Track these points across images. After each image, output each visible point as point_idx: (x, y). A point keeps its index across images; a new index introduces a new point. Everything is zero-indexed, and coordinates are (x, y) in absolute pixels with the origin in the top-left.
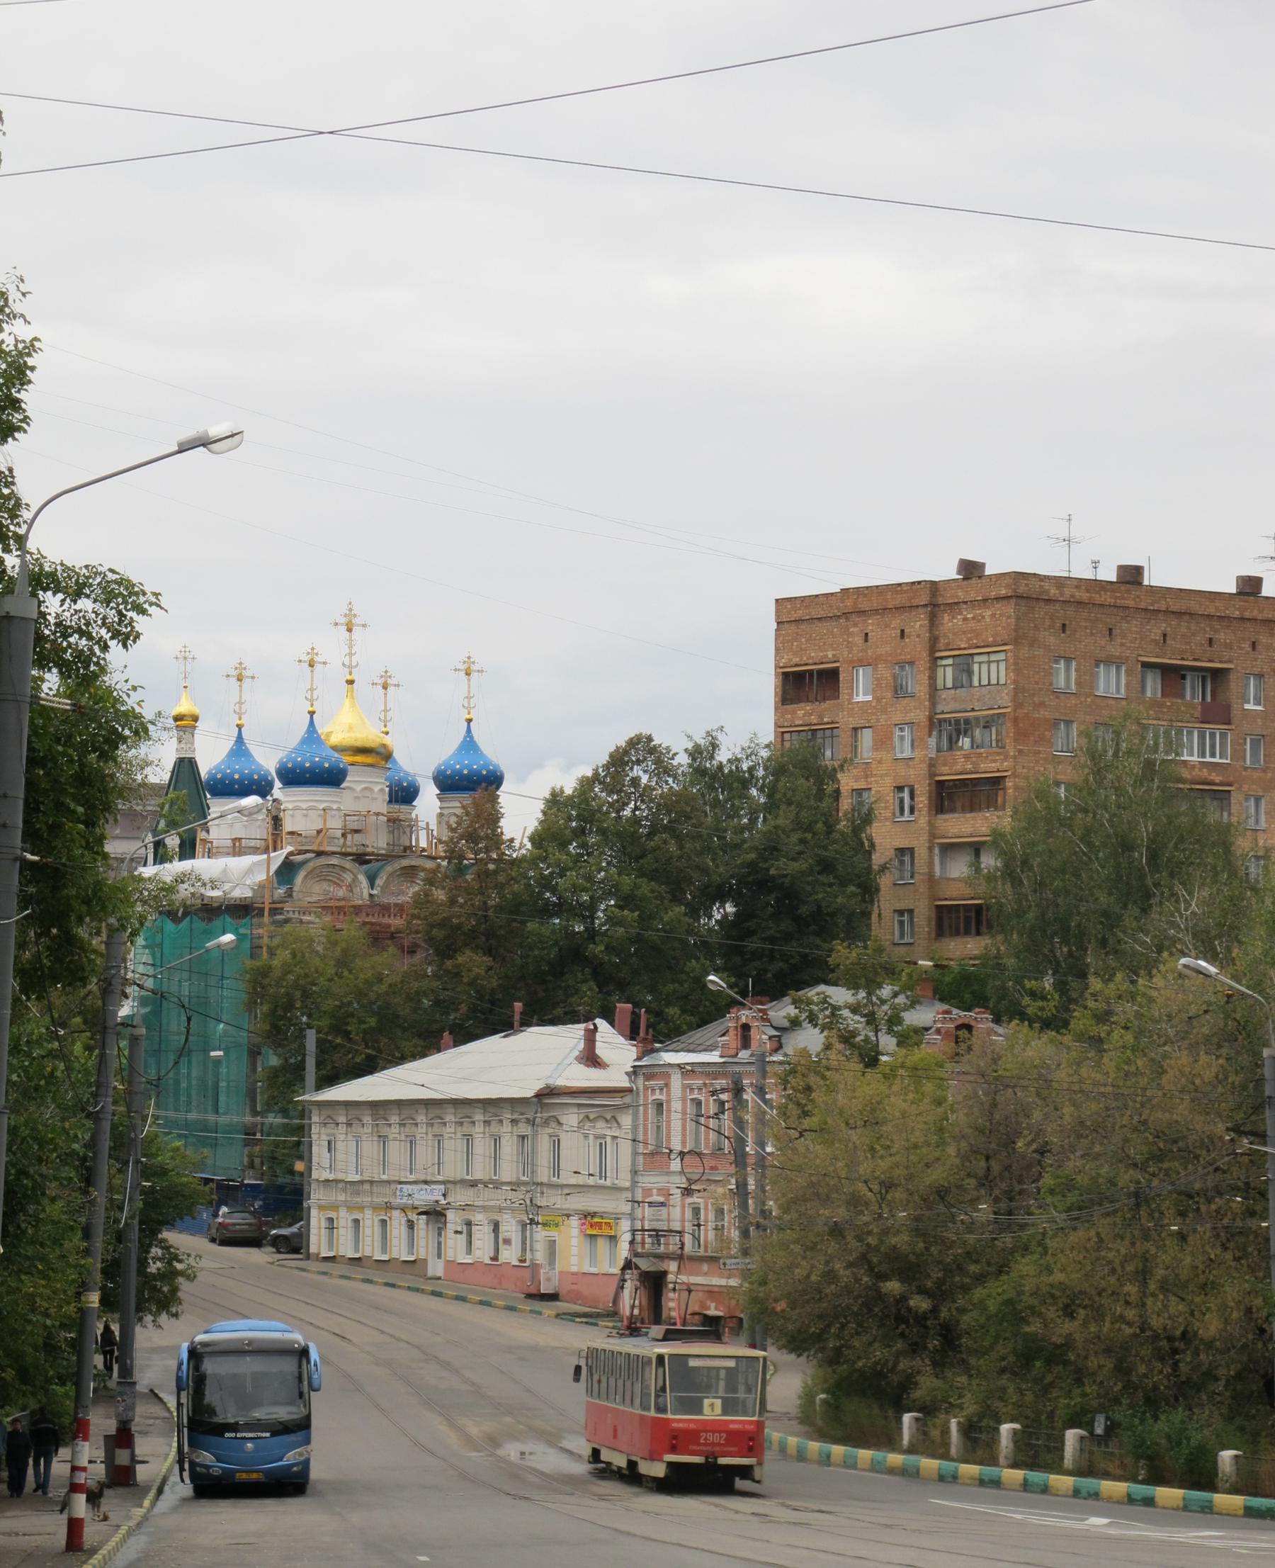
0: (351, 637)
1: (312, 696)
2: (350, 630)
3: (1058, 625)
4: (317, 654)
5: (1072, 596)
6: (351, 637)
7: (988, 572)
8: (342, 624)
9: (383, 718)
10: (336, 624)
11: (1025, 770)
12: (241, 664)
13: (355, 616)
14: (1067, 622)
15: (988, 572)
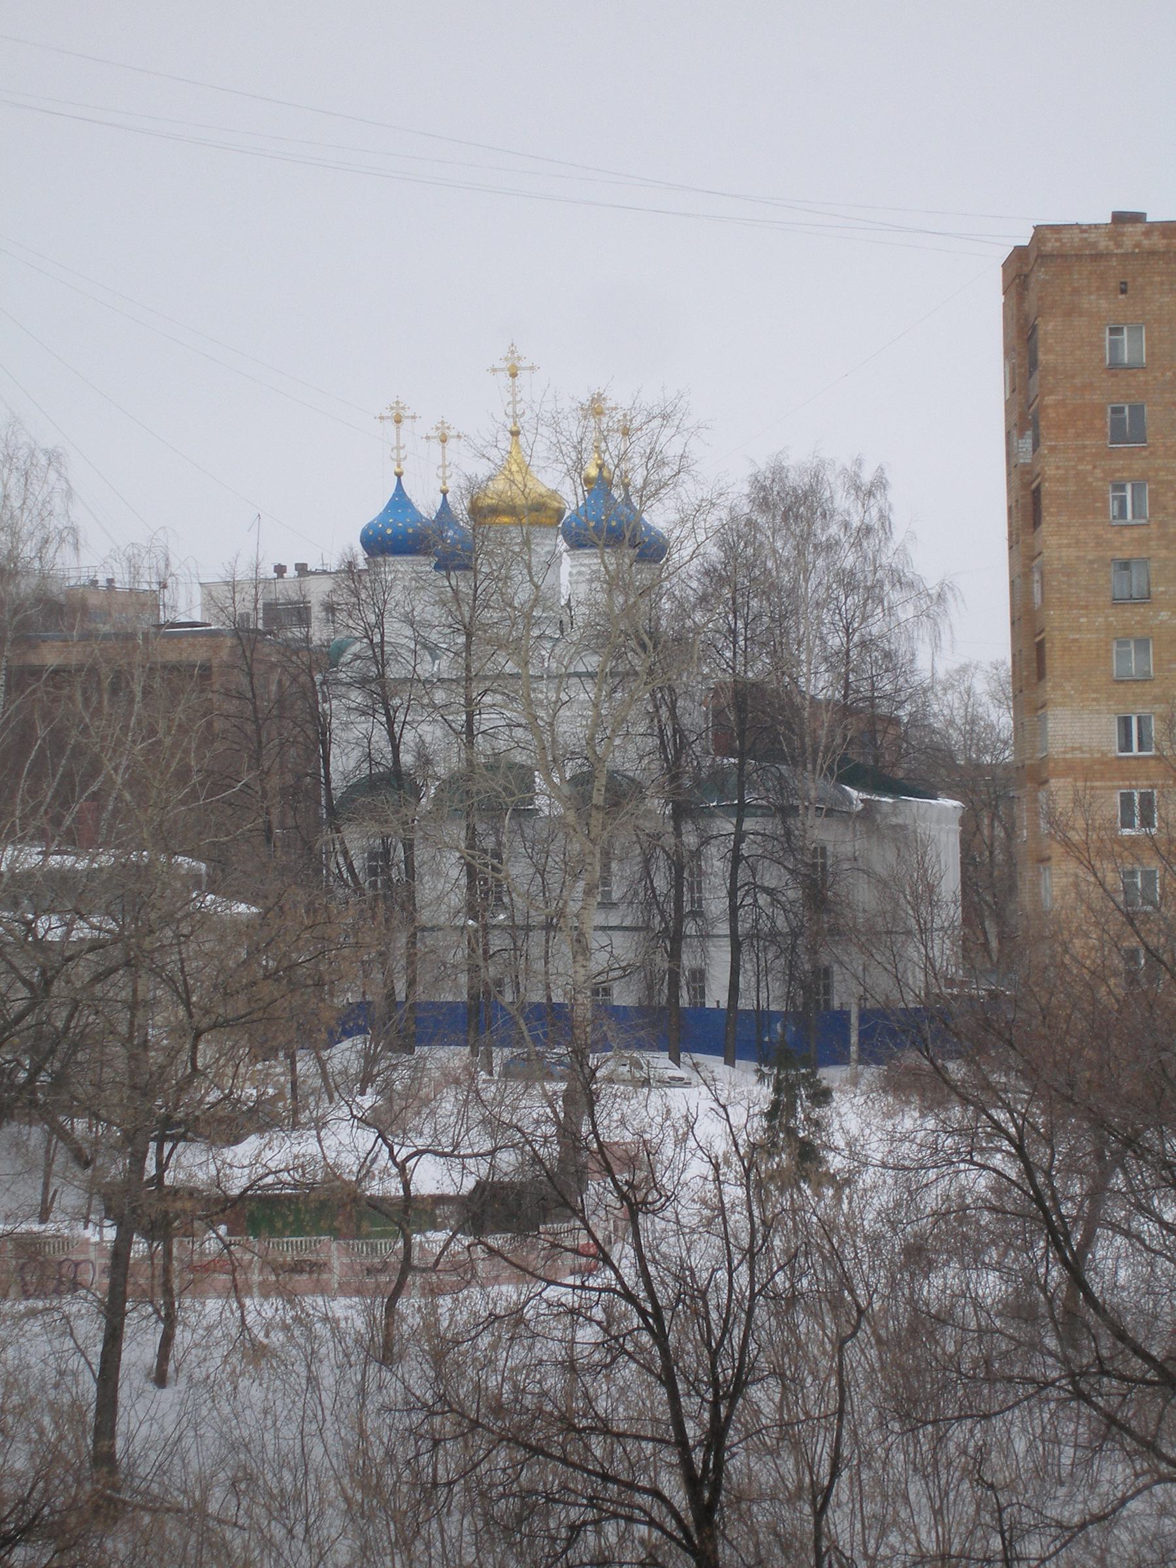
0: (514, 383)
1: (398, 455)
2: (514, 375)
3: (1113, 283)
4: (403, 408)
5: (1137, 245)
6: (514, 383)
7: (1148, 220)
8: (502, 370)
9: (441, 474)
10: (494, 370)
11: (1061, 472)
12: (443, 423)
13: (519, 358)
14: (1129, 280)
15: (1148, 220)
